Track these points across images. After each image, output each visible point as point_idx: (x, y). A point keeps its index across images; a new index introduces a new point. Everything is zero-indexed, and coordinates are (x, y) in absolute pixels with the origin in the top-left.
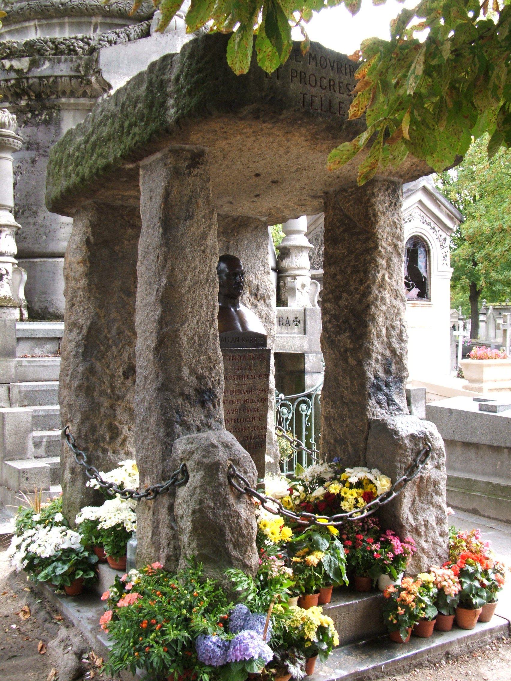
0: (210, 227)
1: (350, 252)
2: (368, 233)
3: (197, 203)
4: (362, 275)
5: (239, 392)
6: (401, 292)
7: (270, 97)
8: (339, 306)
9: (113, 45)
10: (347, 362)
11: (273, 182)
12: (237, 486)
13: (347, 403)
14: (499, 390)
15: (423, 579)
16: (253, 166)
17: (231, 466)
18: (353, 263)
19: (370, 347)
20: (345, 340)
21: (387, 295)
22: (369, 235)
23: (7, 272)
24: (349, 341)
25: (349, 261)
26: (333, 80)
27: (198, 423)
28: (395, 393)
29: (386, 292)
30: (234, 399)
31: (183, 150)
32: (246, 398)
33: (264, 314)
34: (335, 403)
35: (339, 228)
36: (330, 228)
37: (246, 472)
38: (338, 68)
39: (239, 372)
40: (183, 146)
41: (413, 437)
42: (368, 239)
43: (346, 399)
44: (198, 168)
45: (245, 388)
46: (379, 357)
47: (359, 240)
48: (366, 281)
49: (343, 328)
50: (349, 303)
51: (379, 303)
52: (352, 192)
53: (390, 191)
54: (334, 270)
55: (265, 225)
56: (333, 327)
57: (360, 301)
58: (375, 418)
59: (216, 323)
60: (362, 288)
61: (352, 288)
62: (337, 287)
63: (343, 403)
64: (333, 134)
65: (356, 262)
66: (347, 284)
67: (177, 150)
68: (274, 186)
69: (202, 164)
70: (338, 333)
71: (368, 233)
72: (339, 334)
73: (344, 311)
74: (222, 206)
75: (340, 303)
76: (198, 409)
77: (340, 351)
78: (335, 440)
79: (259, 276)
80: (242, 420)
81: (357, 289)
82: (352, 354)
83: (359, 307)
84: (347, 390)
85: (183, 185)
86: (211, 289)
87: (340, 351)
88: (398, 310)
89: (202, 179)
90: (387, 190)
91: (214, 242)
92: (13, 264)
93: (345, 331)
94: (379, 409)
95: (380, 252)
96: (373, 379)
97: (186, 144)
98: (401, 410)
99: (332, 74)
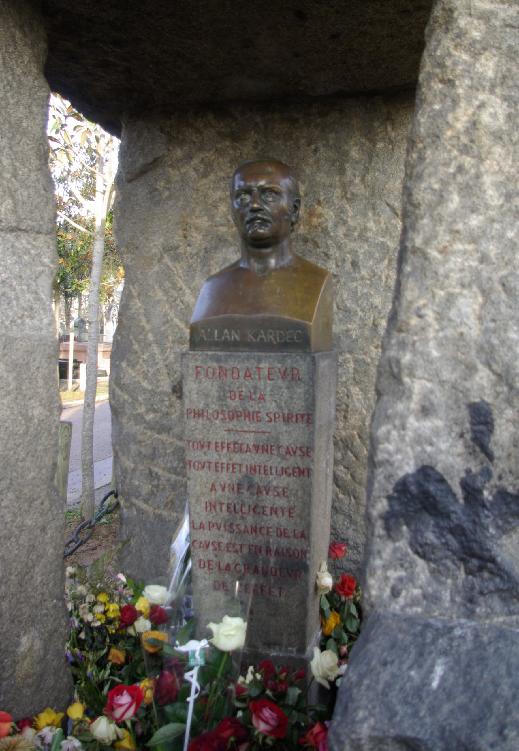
5: (237, 447)
19: (407, 358)
30: (224, 461)
39: (234, 404)
80: (245, 509)
95: (461, 34)
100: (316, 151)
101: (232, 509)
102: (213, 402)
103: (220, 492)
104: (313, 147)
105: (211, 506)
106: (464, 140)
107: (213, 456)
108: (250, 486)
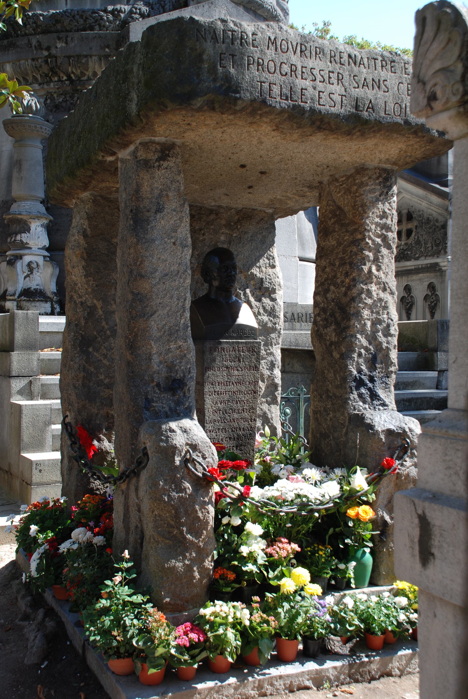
0: (181, 219)
1: (339, 244)
2: (356, 223)
3: (167, 195)
4: (348, 267)
6: (390, 285)
7: (224, 88)
8: (327, 299)
10: (332, 356)
11: (262, 173)
12: (193, 470)
13: (331, 397)
16: (235, 157)
17: (188, 451)
18: (341, 255)
20: (331, 333)
21: (373, 287)
22: (356, 226)
23: (38, 265)
24: (333, 335)
25: (337, 253)
26: (295, 65)
27: (167, 409)
28: (380, 388)
29: (373, 285)
31: (153, 142)
32: (235, 389)
33: (268, 308)
35: (330, 219)
36: (323, 219)
37: (204, 458)
38: (301, 52)
40: (153, 138)
41: (389, 432)
42: (356, 230)
44: (168, 161)
45: (233, 379)
46: (363, 351)
47: (347, 231)
48: (351, 274)
50: (336, 296)
51: (363, 296)
52: (342, 181)
53: (381, 180)
55: (272, 218)
56: (321, 320)
57: (345, 294)
58: (356, 412)
59: (188, 314)
60: (347, 280)
61: (339, 281)
62: (326, 280)
63: (328, 397)
64: (297, 123)
65: (343, 254)
66: (335, 276)
67: (147, 143)
68: (264, 177)
69: (172, 157)
70: (325, 327)
71: (356, 223)
72: (326, 328)
73: (331, 305)
74: (220, 197)
75: (328, 295)
76: (167, 396)
77: (326, 345)
79: (264, 269)
81: (343, 282)
82: (335, 348)
83: (345, 300)
84: (331, 383)
85: (154, 177)
86: (182, 280)
87: (326, 345)
88: (385, 303)
89: (172, 172)
90: (378, 178)
91: (186, 234)
92: (45, 257)
93: (331, 323)
94: (361, 404)
96: (355, 372)
97: (155, 136)
98: (387, 406)
99: (295, 59)
100: (203, 235)
104: (203, 232)
106: (367, 276)
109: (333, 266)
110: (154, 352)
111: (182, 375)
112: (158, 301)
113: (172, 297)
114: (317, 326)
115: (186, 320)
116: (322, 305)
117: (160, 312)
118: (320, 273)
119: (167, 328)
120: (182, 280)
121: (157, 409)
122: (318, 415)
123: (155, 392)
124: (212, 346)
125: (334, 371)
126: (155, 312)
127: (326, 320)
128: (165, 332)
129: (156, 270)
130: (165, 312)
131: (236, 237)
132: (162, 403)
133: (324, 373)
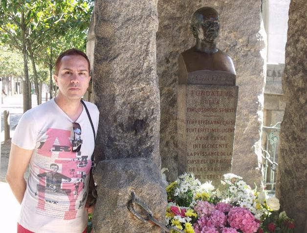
5: (207, 122)
8: (296, 48)
9: (202, 197)
10: (298, 101)
14: (14, 108)
15: (259, 217)
24: (301, 81)
27: (129, 148)
30: (202, 128)
34: (288, 138)
43: (296, 134)
49: (298, 68)
54: (296, 16)
56: (291, 68)
63: (294, 139)
70: (294, 74)
75: (297, 45)
76: (131, 135)
77: (294, 91)
78: (286, 171)
86: (145, 25)
101: (204, 146)
102: (199, 105)
103: (199, 140)
105: (196, 146)
107: (197, 126)
108: (212, 137)
109: (303, 17)
110: (117, 94)
111: (145, 116)
112: (121, 45)
113: (134, 41)
114: (287, 74)
115: (149, 63)
116: (292, 55)
117: (122, 55)
118: (292, 26)
119: (130, 70)
120: (145, 25)
121: (119, 147)
122: (285, 153)
123: (118, 132)
124: (193, 89)
125: (300, 115)
126: (118, 55)
127: (295, 68)
128: (127, 74)
129: (119, 15)
130: (128, 55)
131: (227, 3)
132: (124, 142)
133: (291, 117)
